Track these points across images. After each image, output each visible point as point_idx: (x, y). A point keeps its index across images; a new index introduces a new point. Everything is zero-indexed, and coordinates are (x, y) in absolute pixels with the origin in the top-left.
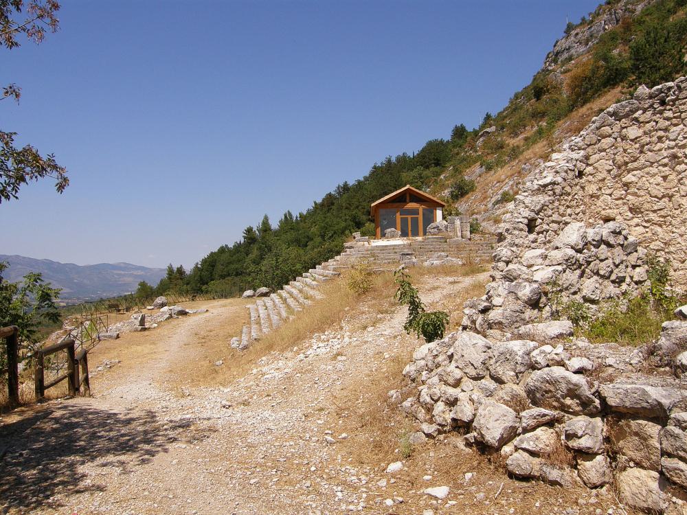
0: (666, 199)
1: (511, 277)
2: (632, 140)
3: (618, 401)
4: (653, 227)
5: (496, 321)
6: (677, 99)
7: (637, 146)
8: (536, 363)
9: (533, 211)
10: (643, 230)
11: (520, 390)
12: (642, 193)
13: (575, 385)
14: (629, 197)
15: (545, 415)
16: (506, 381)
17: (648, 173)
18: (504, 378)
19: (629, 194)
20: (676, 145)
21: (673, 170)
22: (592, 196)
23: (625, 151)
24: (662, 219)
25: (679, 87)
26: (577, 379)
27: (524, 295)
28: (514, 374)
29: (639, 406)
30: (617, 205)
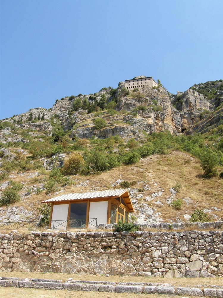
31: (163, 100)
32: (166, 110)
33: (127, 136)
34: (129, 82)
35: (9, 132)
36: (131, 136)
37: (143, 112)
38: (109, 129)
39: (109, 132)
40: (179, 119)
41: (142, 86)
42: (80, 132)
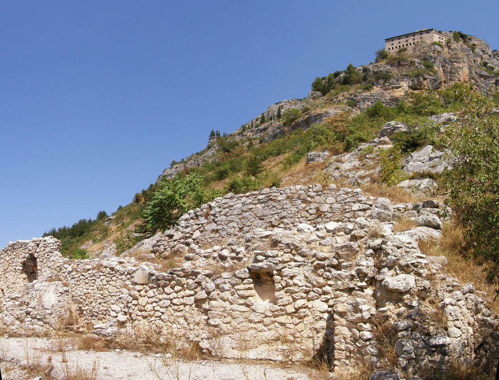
31: (452, 60)
32: (456, 75)
34: (393, 40)
42: (270, 134)
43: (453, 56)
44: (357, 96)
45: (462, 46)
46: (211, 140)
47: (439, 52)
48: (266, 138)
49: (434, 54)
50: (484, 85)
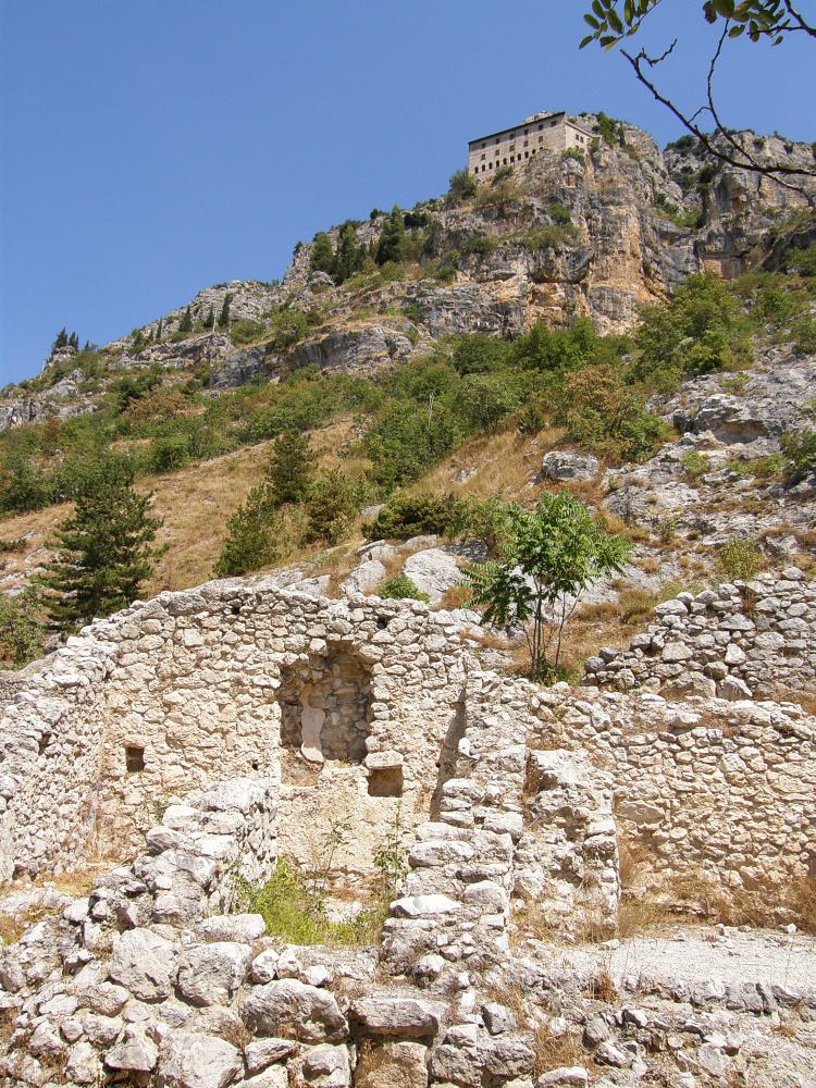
0: (219, 735)
1: (161, 845)
2: (187, 647)
3: (382, 1020)
4: (195, 770)
5: (171, 912)
6: (254, 611)
7: (194, 656)
8: (262, 975)
9: (49, 721)
10: (182, 771)
11: (232, 1014)
12: (188, 720)
13: (324, 1003)
14: (169, 723)
15: (283, 1048)
16: (211, 1002)
17: (200, 696)
18: (207, 998)
19: (170, 718)
20: (244, 668)
21: (234, 698)
22: (115, 711)
23: (175, 659)
24: (210, 761)
25: (259, 598)
26: (324, 995)
27: (203, 875)
28: (226, 991)
29: (408, 1025)
30: (150, 730)
31: (606, 199)
33: (364, 363)
35: (70, 387)
36: (378, 359)
37: (480, 261)
38: (312, 346)
39: (310, 354)
40: (687, 261)
41: (527, 154)
42: (233, 367)
43: (607, 187)
44: (426, 295)
45: (619, 156)
46: (56, 357)
47: (579, 178)
48: (221, 375)
49: (569, 184)
50: (670, 260)
